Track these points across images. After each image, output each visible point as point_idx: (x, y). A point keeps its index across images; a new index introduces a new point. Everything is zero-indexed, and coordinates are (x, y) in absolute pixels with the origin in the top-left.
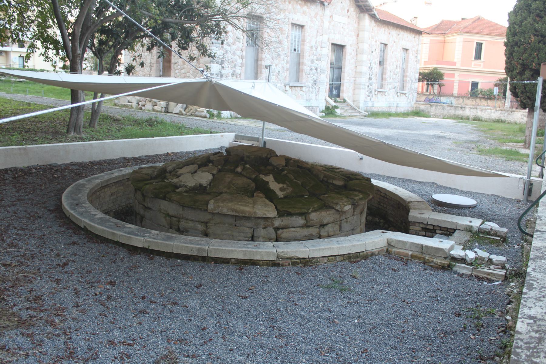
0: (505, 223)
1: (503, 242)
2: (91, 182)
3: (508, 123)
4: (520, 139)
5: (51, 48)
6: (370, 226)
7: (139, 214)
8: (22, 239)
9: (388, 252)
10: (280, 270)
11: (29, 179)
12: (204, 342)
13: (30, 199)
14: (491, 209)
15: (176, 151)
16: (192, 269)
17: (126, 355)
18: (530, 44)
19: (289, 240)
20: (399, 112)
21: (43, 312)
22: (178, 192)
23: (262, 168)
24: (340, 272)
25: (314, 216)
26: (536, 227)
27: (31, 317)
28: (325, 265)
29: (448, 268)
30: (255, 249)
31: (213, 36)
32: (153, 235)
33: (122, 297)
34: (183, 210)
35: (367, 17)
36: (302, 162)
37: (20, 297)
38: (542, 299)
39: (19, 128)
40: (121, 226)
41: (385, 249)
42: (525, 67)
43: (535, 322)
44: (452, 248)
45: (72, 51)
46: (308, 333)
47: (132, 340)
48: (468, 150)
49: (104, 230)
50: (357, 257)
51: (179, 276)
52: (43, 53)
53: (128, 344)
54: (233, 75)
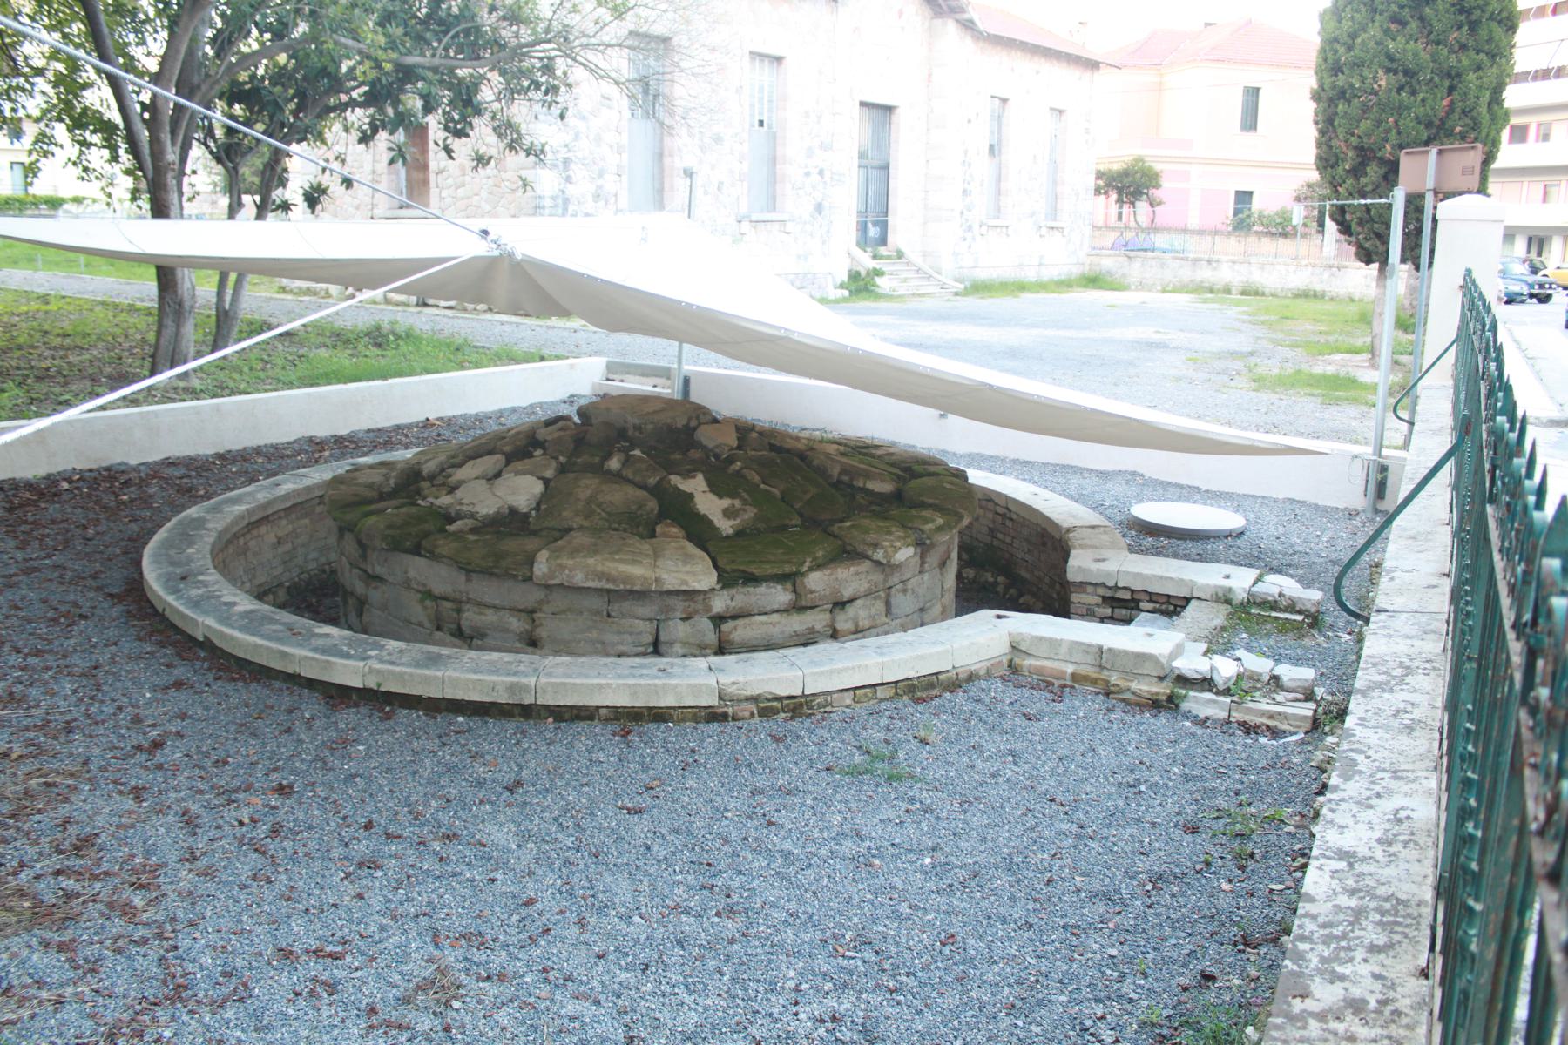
0: (1319, 575)
1: (1311, 626)
2: (221, 511)
3: (1332, 299)
4: (1359, 342)
5: (95, 145)
6: (971, 597)
7: (352, 594)
8: (37, 680)
9: (1013, 668)
10: (728, 730)
11: (51, 511)
12: (530, 938)
13: (56, 567)
14: (1283, 539)
15: (449, 411)
16: (497, 739)
17: (324, 983)
18: (1376, 94)
19: (752, 649)
20: (1045, 279)
21: (99, 880)
22: (454, 534)
23: (677, 456)
24: (888, 728)
25: (816, 581)
26: (1377, 601)
27: (69, 896)
28: (848, 710)
29: (1170, 704)
30: (660, 678)
31: (539, 95)
32: (389, 654)
33: (310, 827)
34: (468, 580)
35: (950, 27)
36: (785, 435)
37: (36, 842)
38: (1374, 802)
39: (18, 368)
40: (303, 632)
41: (1005, 660)
42: (1365, 155)
43: (1351, 865)
44: (1178, 651)
45: (153, 154)
46: (801, 901)
47: (339, 943)
48: (1226, 378)
49: (256, 646)
50: (931, 686)
51: (461, 761)
52: (74, 159)
53: (330, 955)
54: (597, 197)
